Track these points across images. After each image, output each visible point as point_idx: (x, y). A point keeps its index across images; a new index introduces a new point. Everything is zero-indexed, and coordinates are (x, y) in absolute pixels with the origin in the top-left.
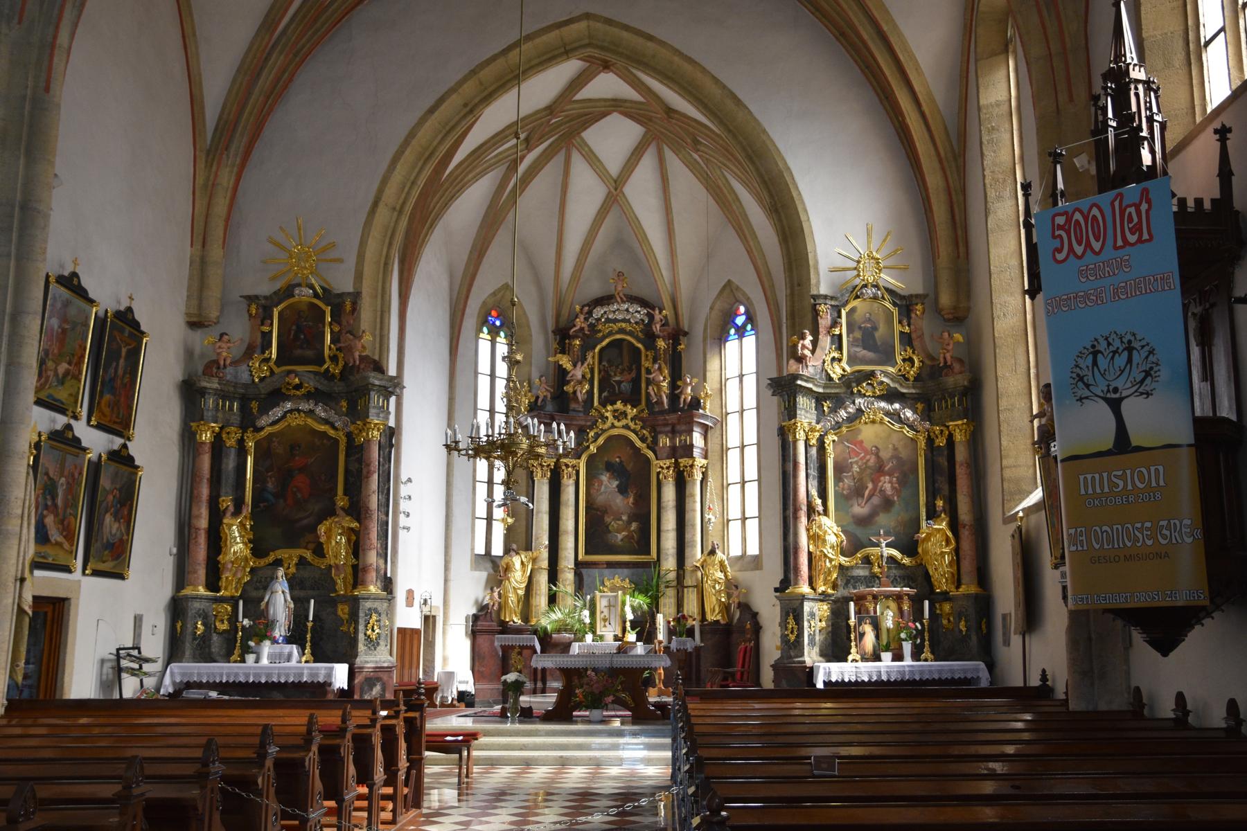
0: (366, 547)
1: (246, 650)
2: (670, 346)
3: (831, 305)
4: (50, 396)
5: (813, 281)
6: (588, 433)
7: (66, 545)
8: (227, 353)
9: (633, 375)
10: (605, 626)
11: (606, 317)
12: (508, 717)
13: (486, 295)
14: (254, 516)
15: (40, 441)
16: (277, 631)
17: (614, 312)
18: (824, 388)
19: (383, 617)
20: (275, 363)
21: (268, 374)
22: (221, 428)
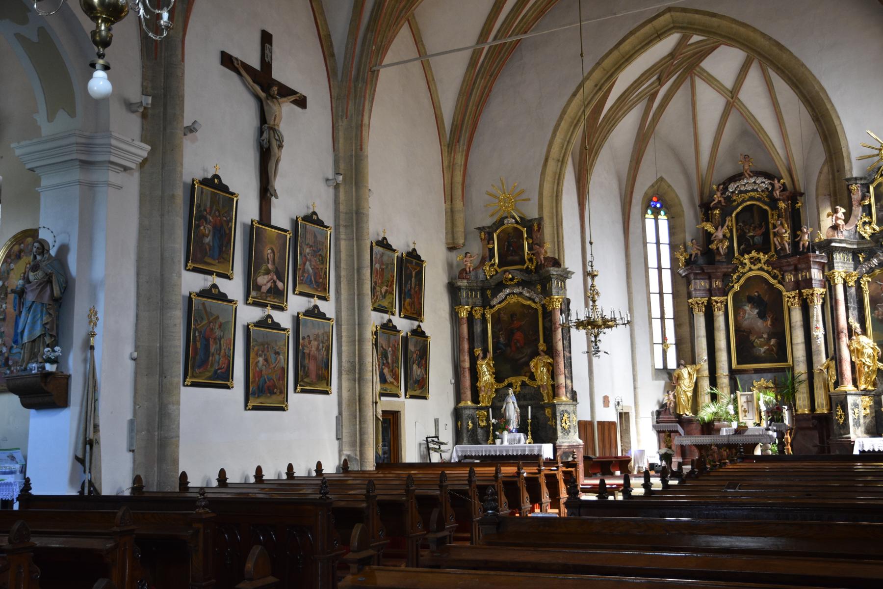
1: (495, 437)
3: (861, 184)
4: (380, 305)
5: (847, 167)
6: (732, 277)
7: (395, 383)
8: (470, 264)
9: (763, 230)
10: (745, 416)
13: (646, 188)
14: (494, 359)
15: (377, 330)
16: (511, 425)
17: (745, 185)
18: (857, 245)
19: (572, 415)
21: (494, 273)
22: (472, 308)
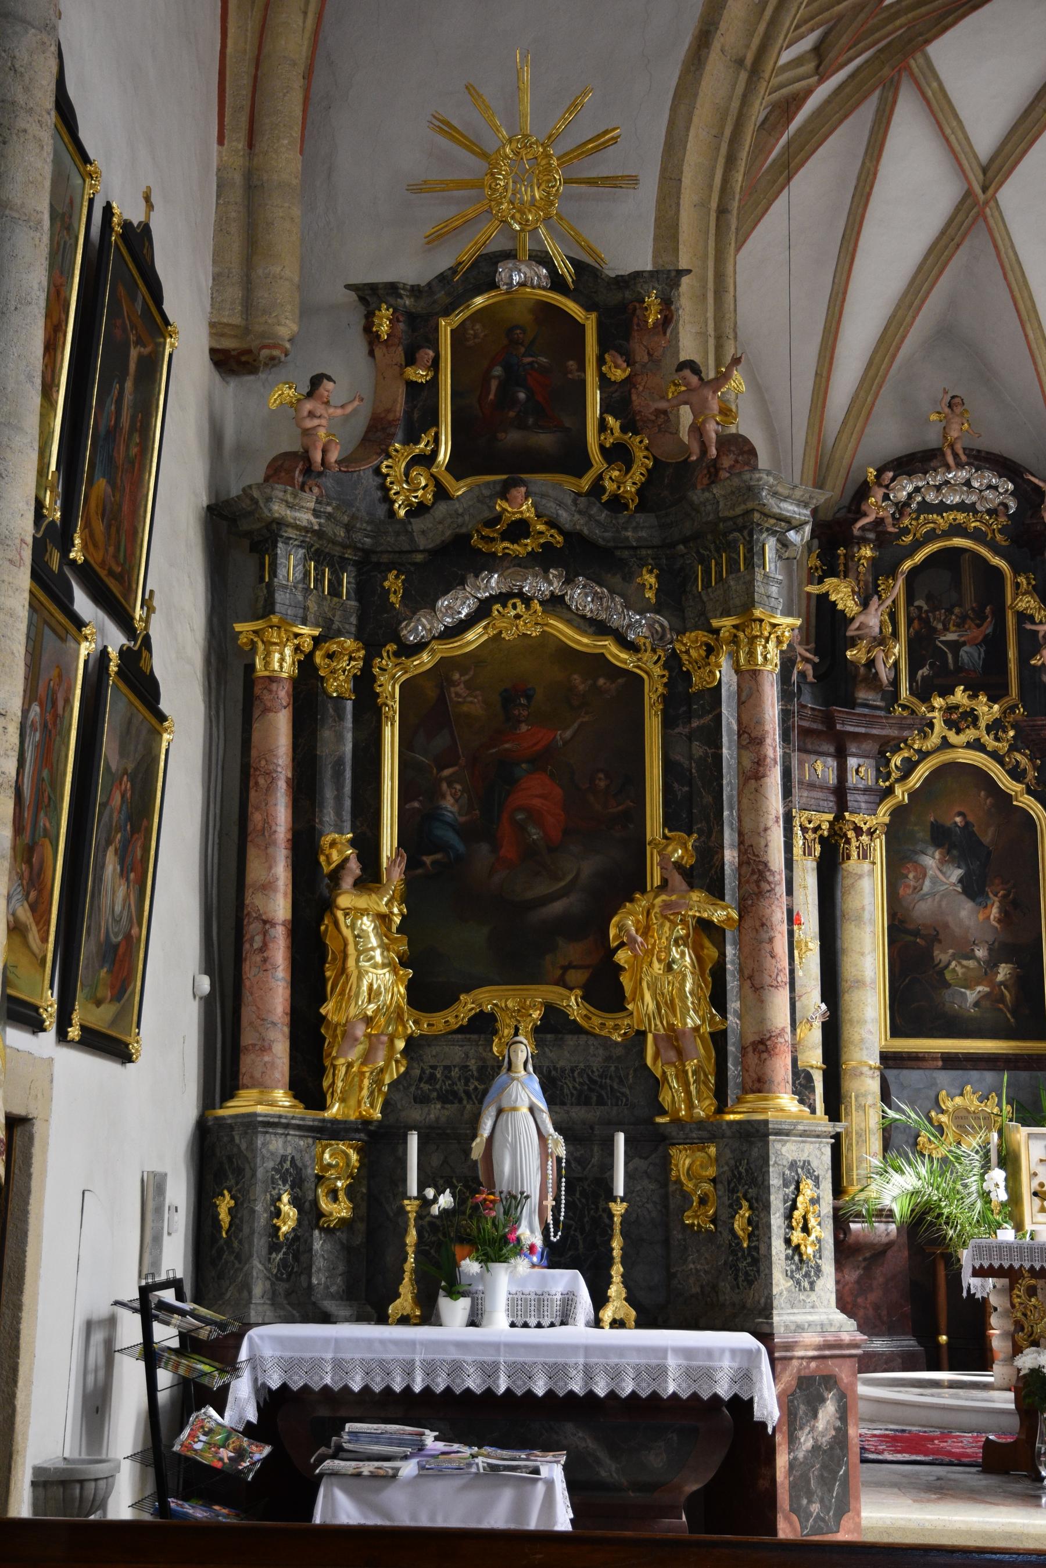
0: (768, 980)
6: (889, 760)
9: (988, 628)
11: (919, 499)
14: (410, 895)
17: (938, 488)
20: (448, 468)
22: (317, 641)
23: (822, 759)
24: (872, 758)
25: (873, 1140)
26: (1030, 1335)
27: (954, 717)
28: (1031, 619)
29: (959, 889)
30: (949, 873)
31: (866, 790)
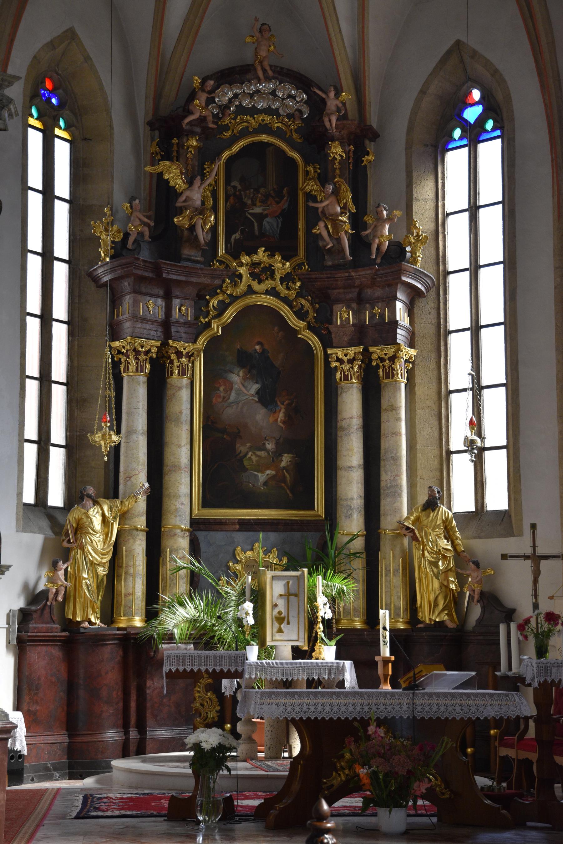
2: (351, 154)
6: (208, 302)
9: (285, 204)
10: (280, 631)
11: (237, 103)
12: (199, 822)
13: (39, 45)
17: (251, 96)
23: (153, 299)
24: (191, 299)
25: (181, 583)
26: (205, 720)
27: (257, 270)
28: (314, 199)
29: (256, 399)
30: (249, 386)
31: (187, 324)
